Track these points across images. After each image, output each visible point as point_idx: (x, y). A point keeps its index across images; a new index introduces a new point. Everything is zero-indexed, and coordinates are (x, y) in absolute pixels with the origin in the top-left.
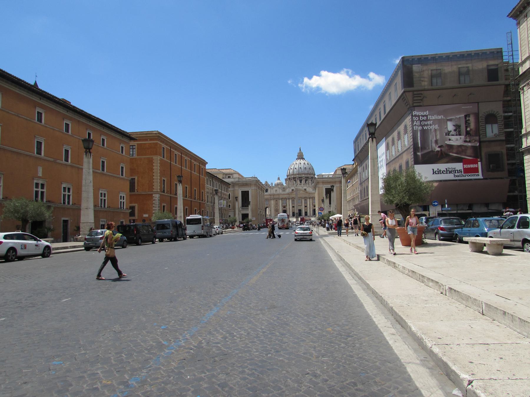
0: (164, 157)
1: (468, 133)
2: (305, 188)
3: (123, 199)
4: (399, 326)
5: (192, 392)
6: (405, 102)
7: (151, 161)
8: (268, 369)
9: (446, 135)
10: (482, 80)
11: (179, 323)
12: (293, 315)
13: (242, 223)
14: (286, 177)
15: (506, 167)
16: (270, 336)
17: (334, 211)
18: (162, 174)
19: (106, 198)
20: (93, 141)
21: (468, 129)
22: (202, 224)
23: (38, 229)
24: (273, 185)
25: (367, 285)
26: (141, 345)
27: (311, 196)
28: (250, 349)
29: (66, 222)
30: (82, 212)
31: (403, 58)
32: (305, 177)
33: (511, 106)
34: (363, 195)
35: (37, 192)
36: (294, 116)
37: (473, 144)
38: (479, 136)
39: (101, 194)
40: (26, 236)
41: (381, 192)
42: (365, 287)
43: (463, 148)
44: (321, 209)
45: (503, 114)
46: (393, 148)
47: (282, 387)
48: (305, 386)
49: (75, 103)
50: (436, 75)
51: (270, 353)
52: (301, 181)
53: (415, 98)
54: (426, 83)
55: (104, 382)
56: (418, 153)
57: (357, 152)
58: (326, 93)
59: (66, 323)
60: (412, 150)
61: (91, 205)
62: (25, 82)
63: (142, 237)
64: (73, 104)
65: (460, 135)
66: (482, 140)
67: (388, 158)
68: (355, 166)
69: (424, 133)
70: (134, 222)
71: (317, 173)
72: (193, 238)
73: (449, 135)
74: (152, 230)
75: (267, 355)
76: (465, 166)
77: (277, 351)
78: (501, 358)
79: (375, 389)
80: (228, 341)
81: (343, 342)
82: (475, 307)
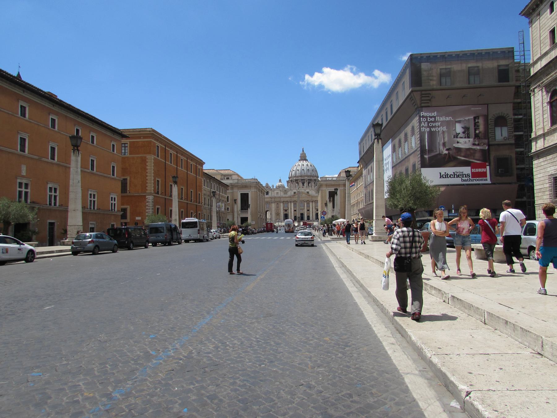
0: (158, 157)
1: (476, 136)
2: (308, 190)
3: (115, 201)
4: (399, 336)
5: (180, 405)
6: (413, 101)
7: (144, 161)
8: (261, 381)
9: (454, 137)
10: (492, 80)
11: (169, 332)
12: (290, 324)
13: (241, 227)
14: (288, 179)
15: (515, 172)
16: (264, 345)
17: (338, 216)
18: (156, 174)
19: (96, 199)
20: (81, 138)
21: (477, 132)
22: (198, 228)
23: (22, 232)
24: (275, 187)
25: (369, 293)
26: (127, 355)
27: (314, 199)
28: (242, 359)
29: (52, 224)
30: (69, 214)
31: (411, 55)
32: (307, 179)
33: (521, 109)
34: (367, 199)
35: (20, 192)
36: (298, 117)
37: (481, 148)
38: (488, 139)
39: (91, 194)
40: (8, 240)
41: (386, 196)
42: (366, 294)
43: (472, 151)
44: (324, 213)
45: (513, 117)
46: (400, 150)
47: (274, 398)
48: (299, 398)
49: (61, 97)
50: (445, 74)
51: (263, 364)
52: (303, 184)
53: (423, 99)
54: (435, 83)
55: (86, 394)
56: (425, 156)
57: (363, 154)
58: (329, 90)
59: (48, 332)
60: (419, 152)
61: (79, 207)
62: (7, 73)
63: (134, 241)
64: (60, 97)
65: (468, 137)
66: (491, 143)
67: (394, 160)
68: (359, 168)
69: (432, 135)
70: (126, 225)
71: (320, 175)
72: (188, 242)
73: (457, 138)
74: (145, 234)
75: (260, 365)
76: (473, 170)
77: (272, 362)
78: (501, 369)
79: (371, 400)
80: (220, 351)
81: (341, 352)
82: (477, 316)
